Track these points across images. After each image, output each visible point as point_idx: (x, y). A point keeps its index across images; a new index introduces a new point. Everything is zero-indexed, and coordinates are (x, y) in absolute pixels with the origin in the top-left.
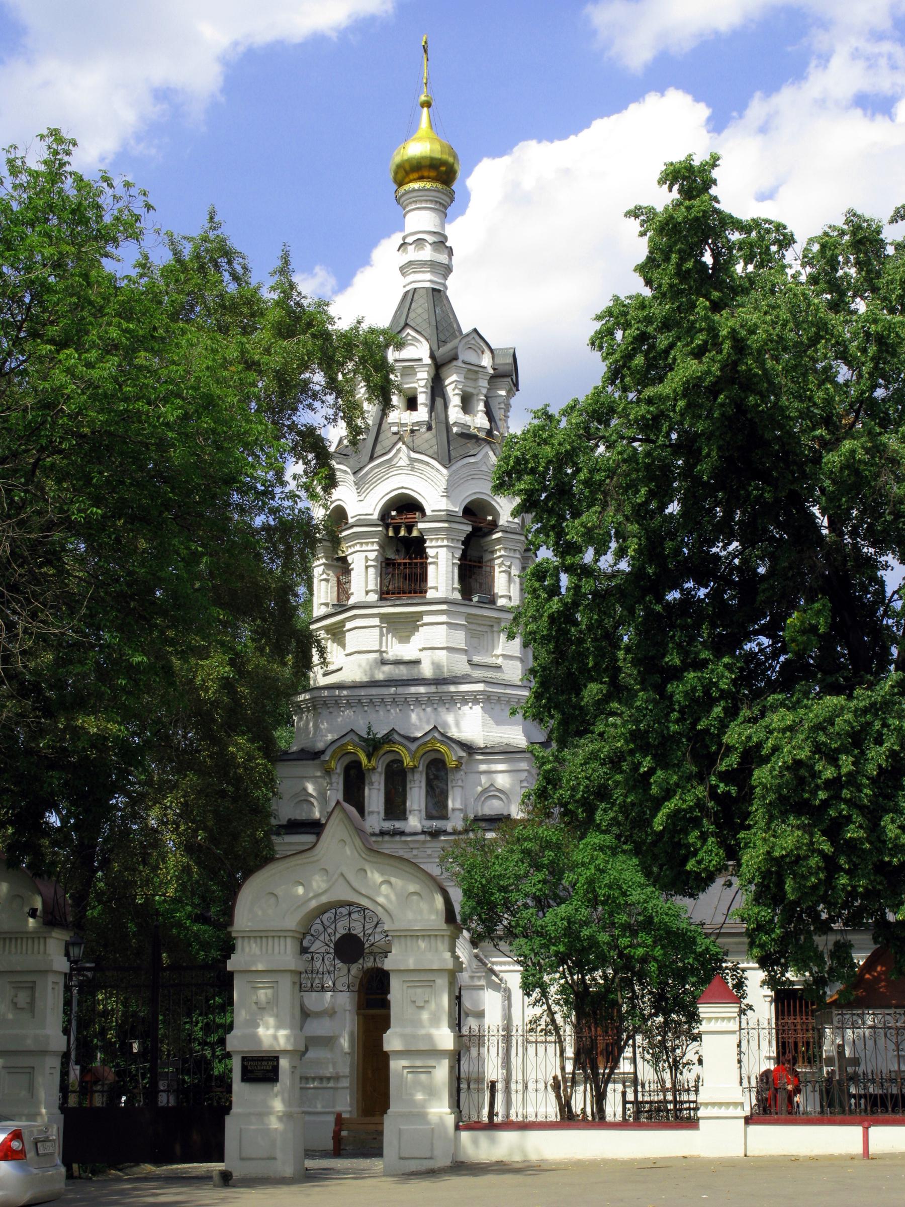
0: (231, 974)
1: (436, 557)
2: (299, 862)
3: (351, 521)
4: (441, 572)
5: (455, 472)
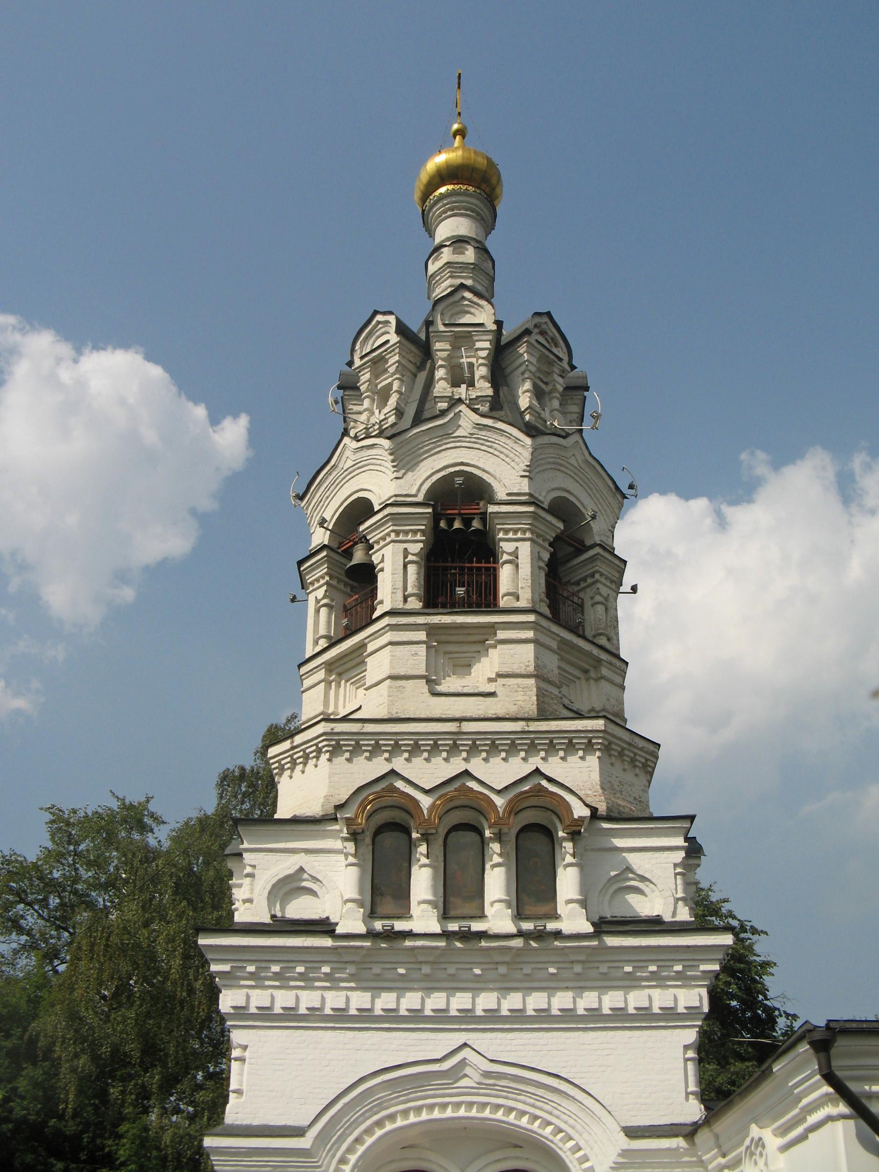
1: (515, 553)
4: (517, 575)
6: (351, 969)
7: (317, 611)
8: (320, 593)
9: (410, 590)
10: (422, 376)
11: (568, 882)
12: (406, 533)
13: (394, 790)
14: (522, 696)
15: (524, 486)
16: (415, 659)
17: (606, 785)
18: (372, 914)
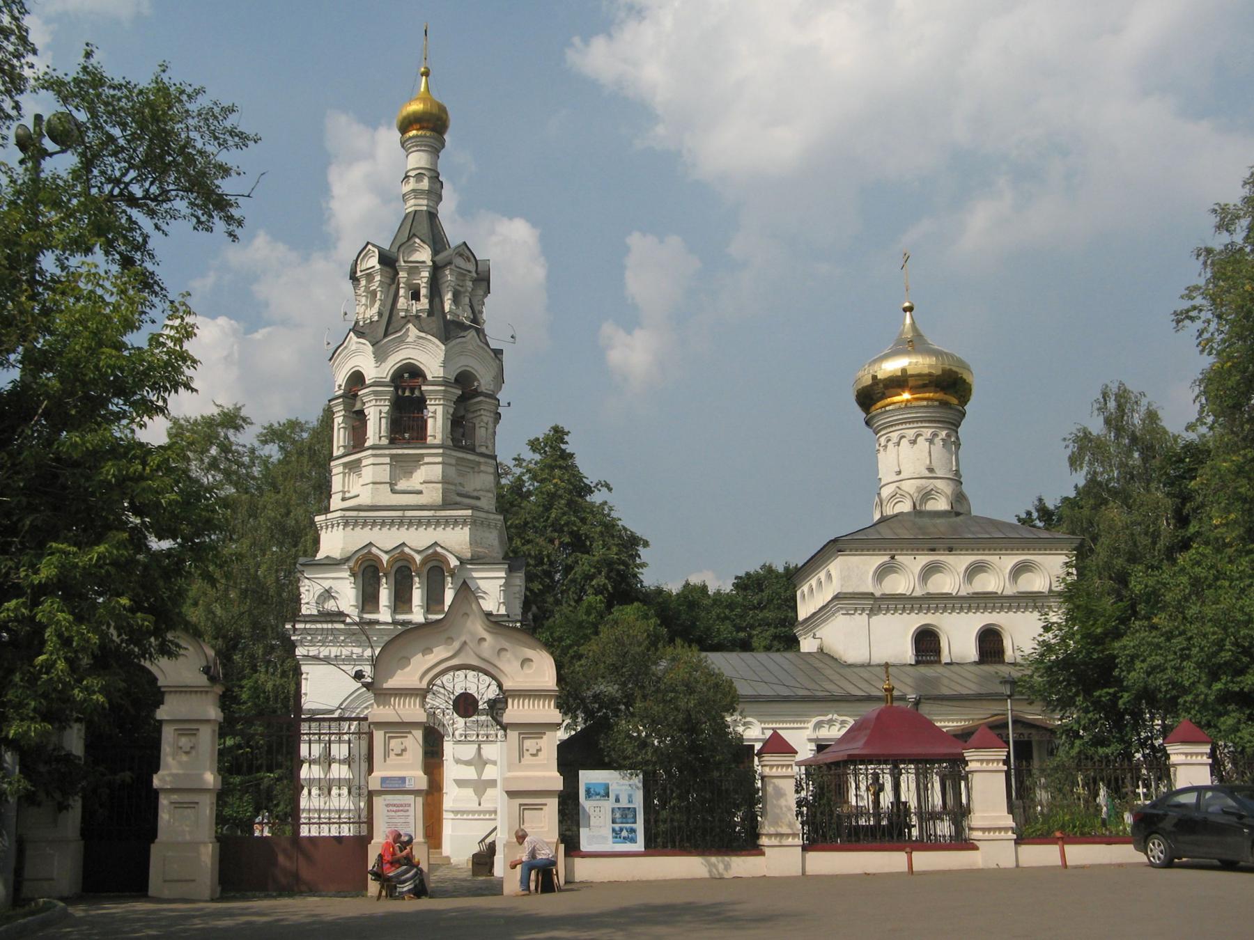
0: (161, 722)
1: (435, 412)
3: (367, 382)
4: (436, 421)
9: (383, 433)
10: (394, 287)
13: (370, 552)
14: (434, 495)
16: (384, 473)
17: (473, 542)
18: (363, 610)
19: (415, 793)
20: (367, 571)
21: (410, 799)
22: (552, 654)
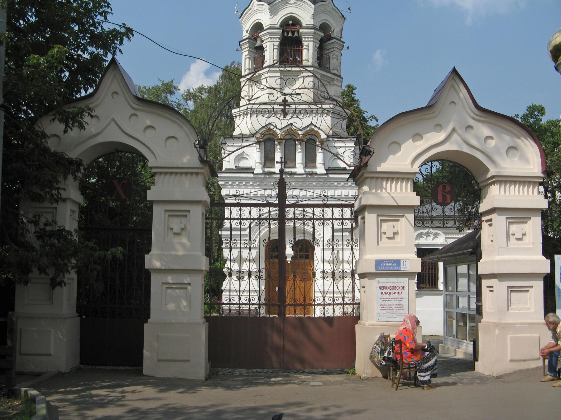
0: (152, 202)
2: (167, 115)
3: (265, 28)
4: (308, 54)
5: (318, 7)
6: (258, 183)
7: (246, 59)
8: (247, 53)
9: (275, 58)
11: (320, 157)
12: (274, 38)
14: (307, 96)
15: (311, 22)
18: (264, 166)
19: (409, 275)
20: (267, 140)
21: (403, 281)
22: (540, 146)
